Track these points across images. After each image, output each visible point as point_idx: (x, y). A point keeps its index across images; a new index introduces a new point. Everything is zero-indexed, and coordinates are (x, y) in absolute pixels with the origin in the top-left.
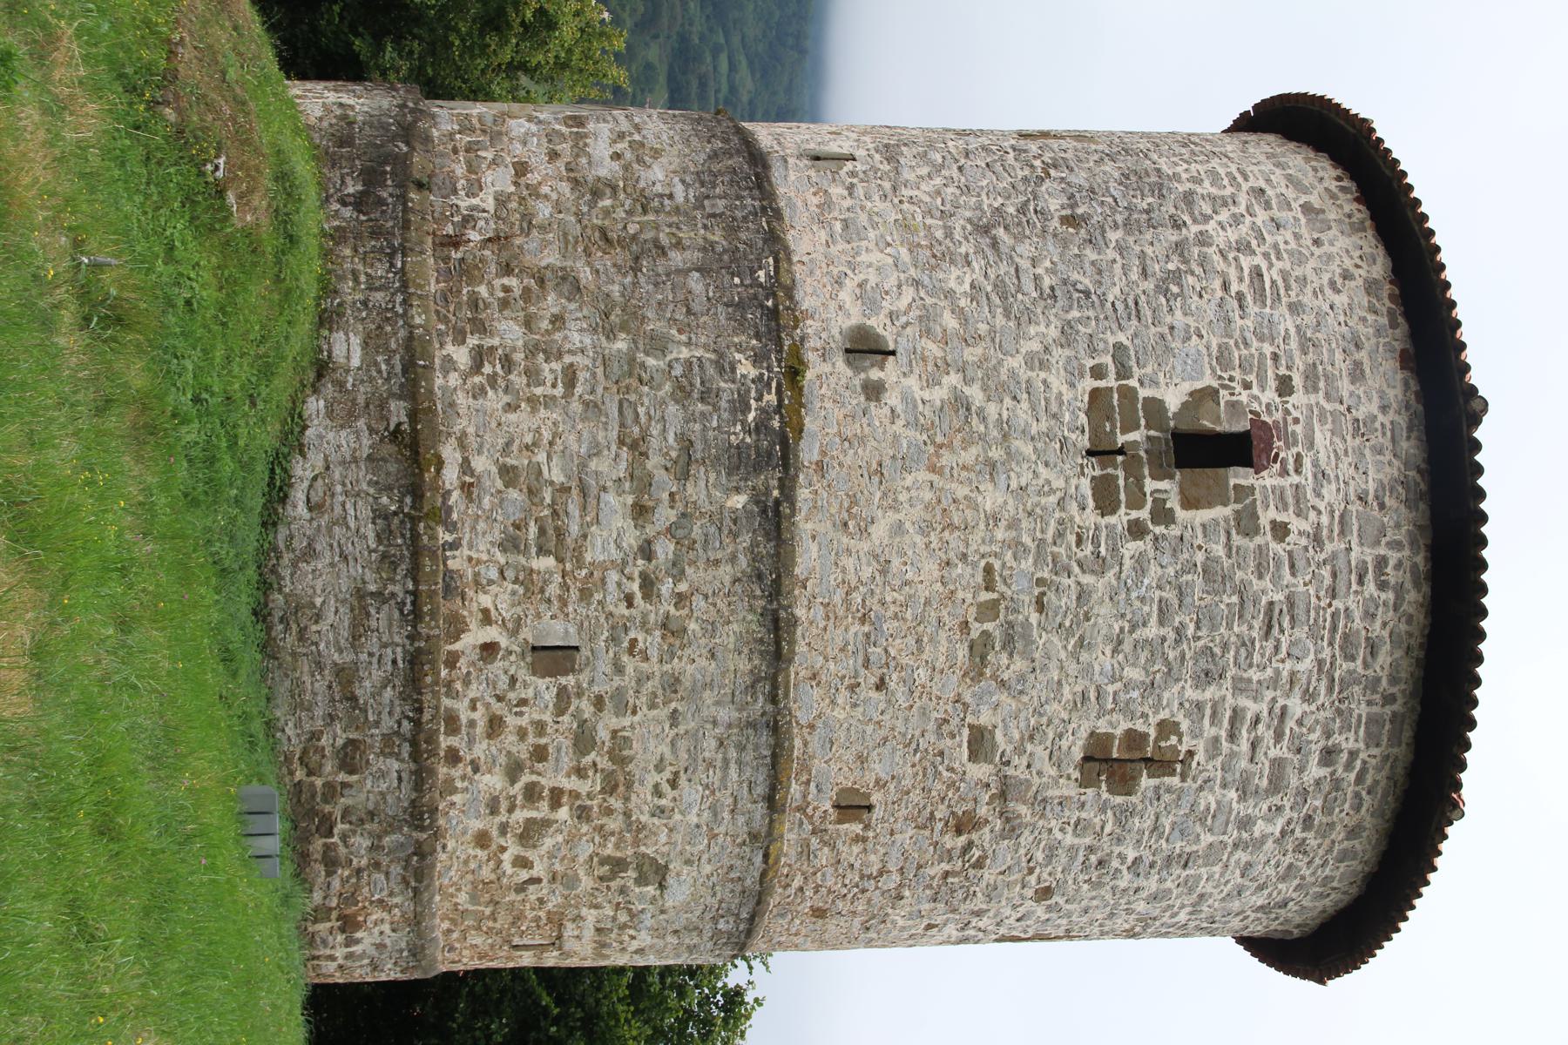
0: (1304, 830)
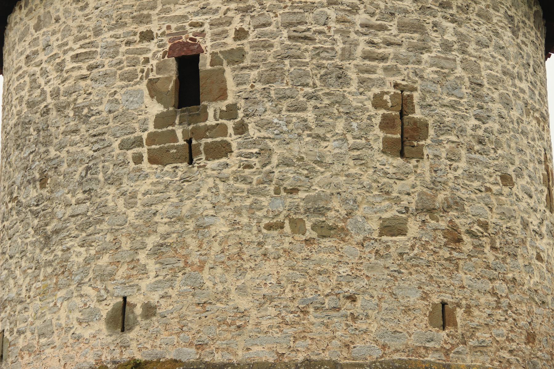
0: (452, 8)
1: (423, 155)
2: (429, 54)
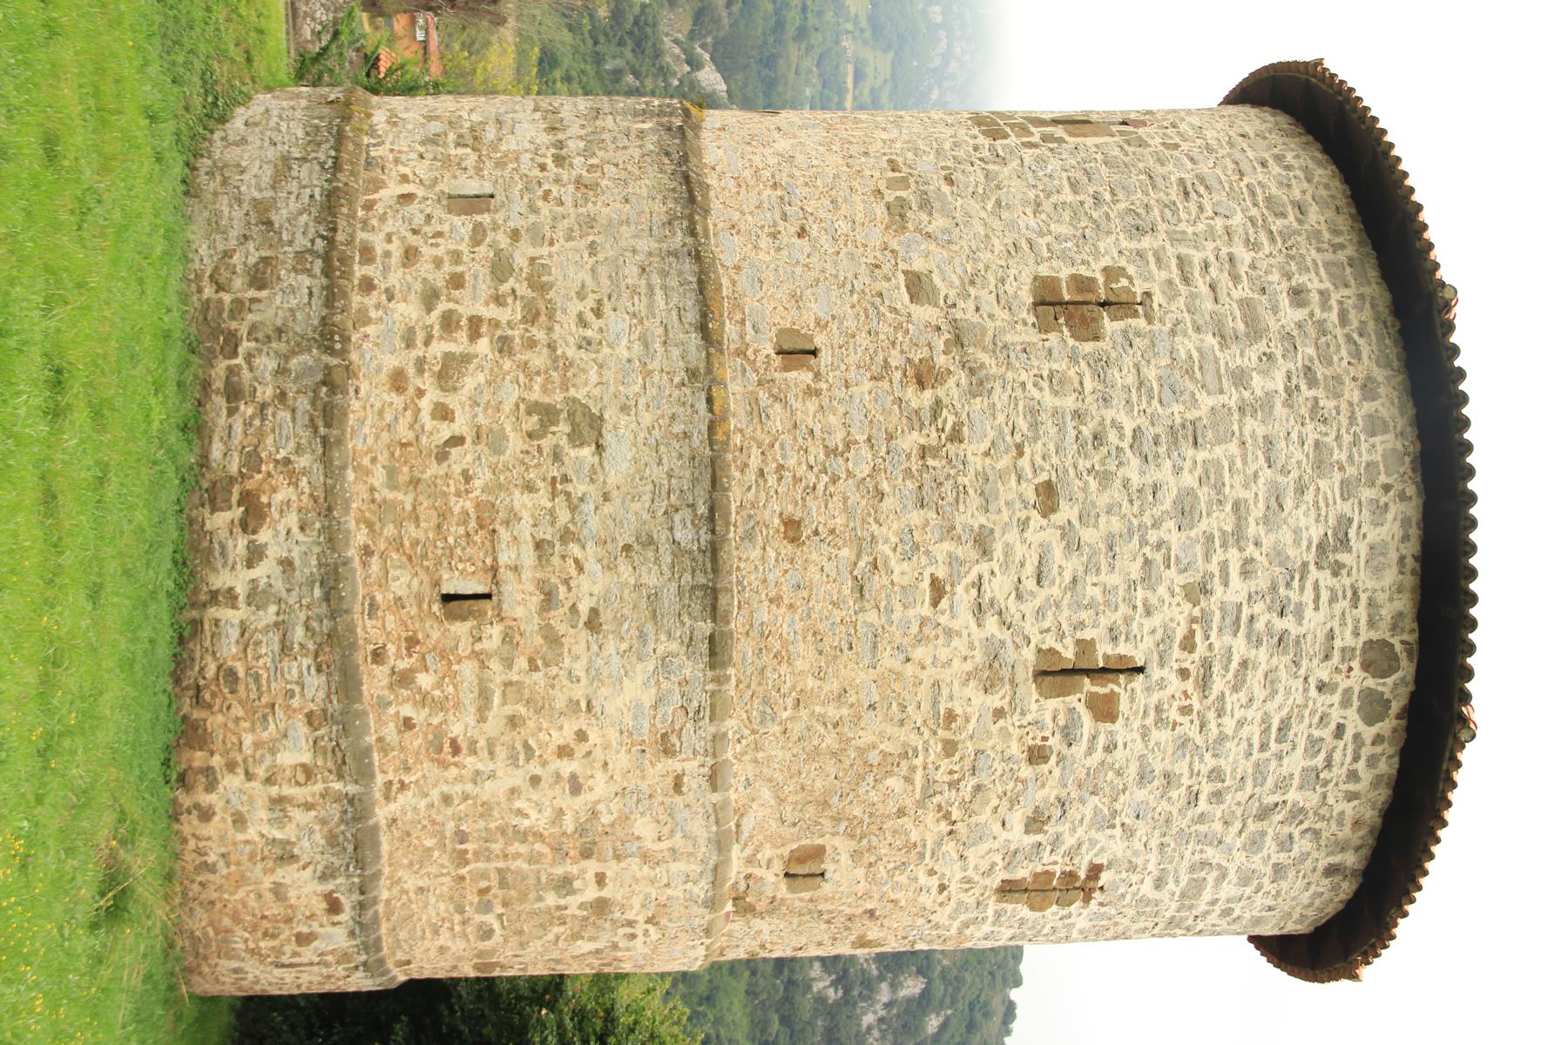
1: (1046, 332)
2: (1217, 347)
